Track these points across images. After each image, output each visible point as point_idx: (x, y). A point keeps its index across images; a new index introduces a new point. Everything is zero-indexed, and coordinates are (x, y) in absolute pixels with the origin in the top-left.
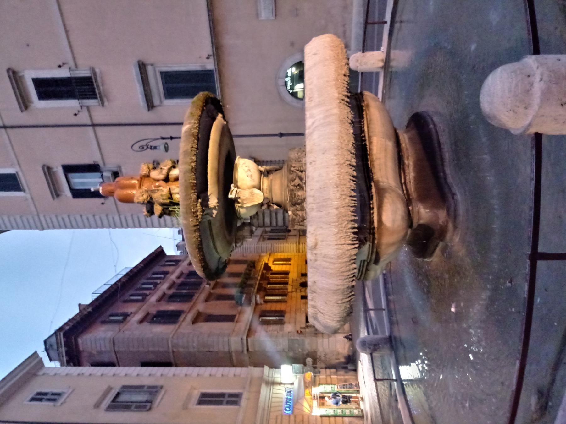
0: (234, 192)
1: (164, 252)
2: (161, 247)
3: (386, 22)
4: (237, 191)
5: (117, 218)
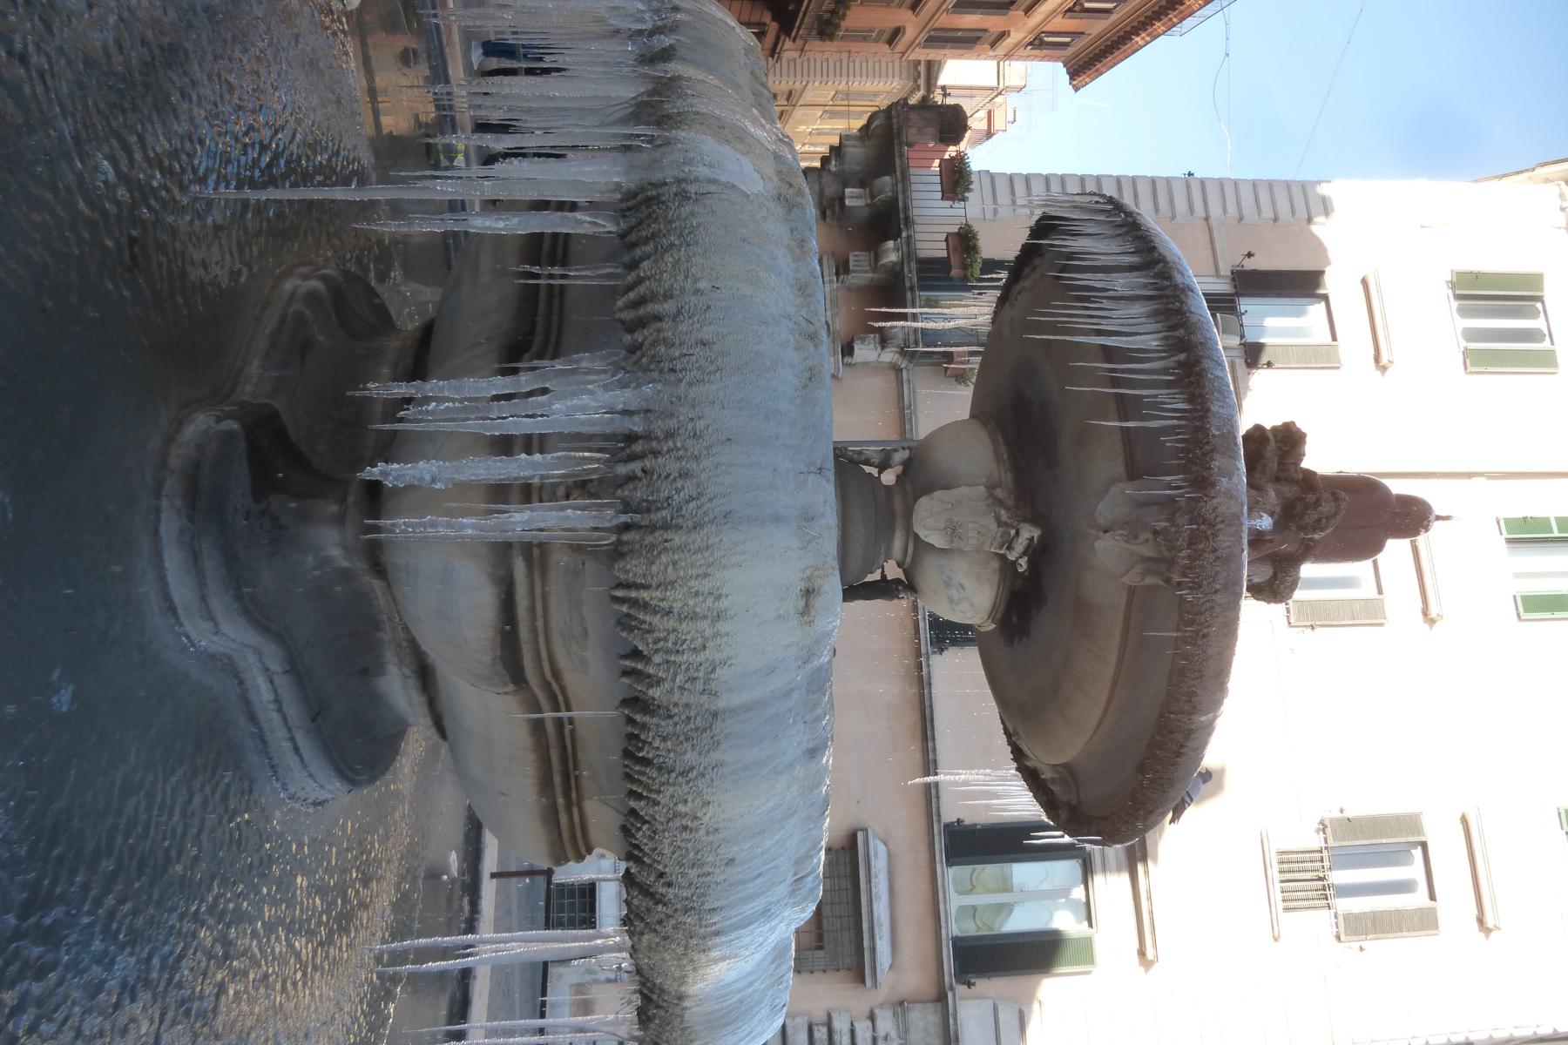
0: (1020, 545)
1: (1068, 73)
2: (1076, 89)
3: (493, 876)
4: (1010, 548)
5: (1215, 209)
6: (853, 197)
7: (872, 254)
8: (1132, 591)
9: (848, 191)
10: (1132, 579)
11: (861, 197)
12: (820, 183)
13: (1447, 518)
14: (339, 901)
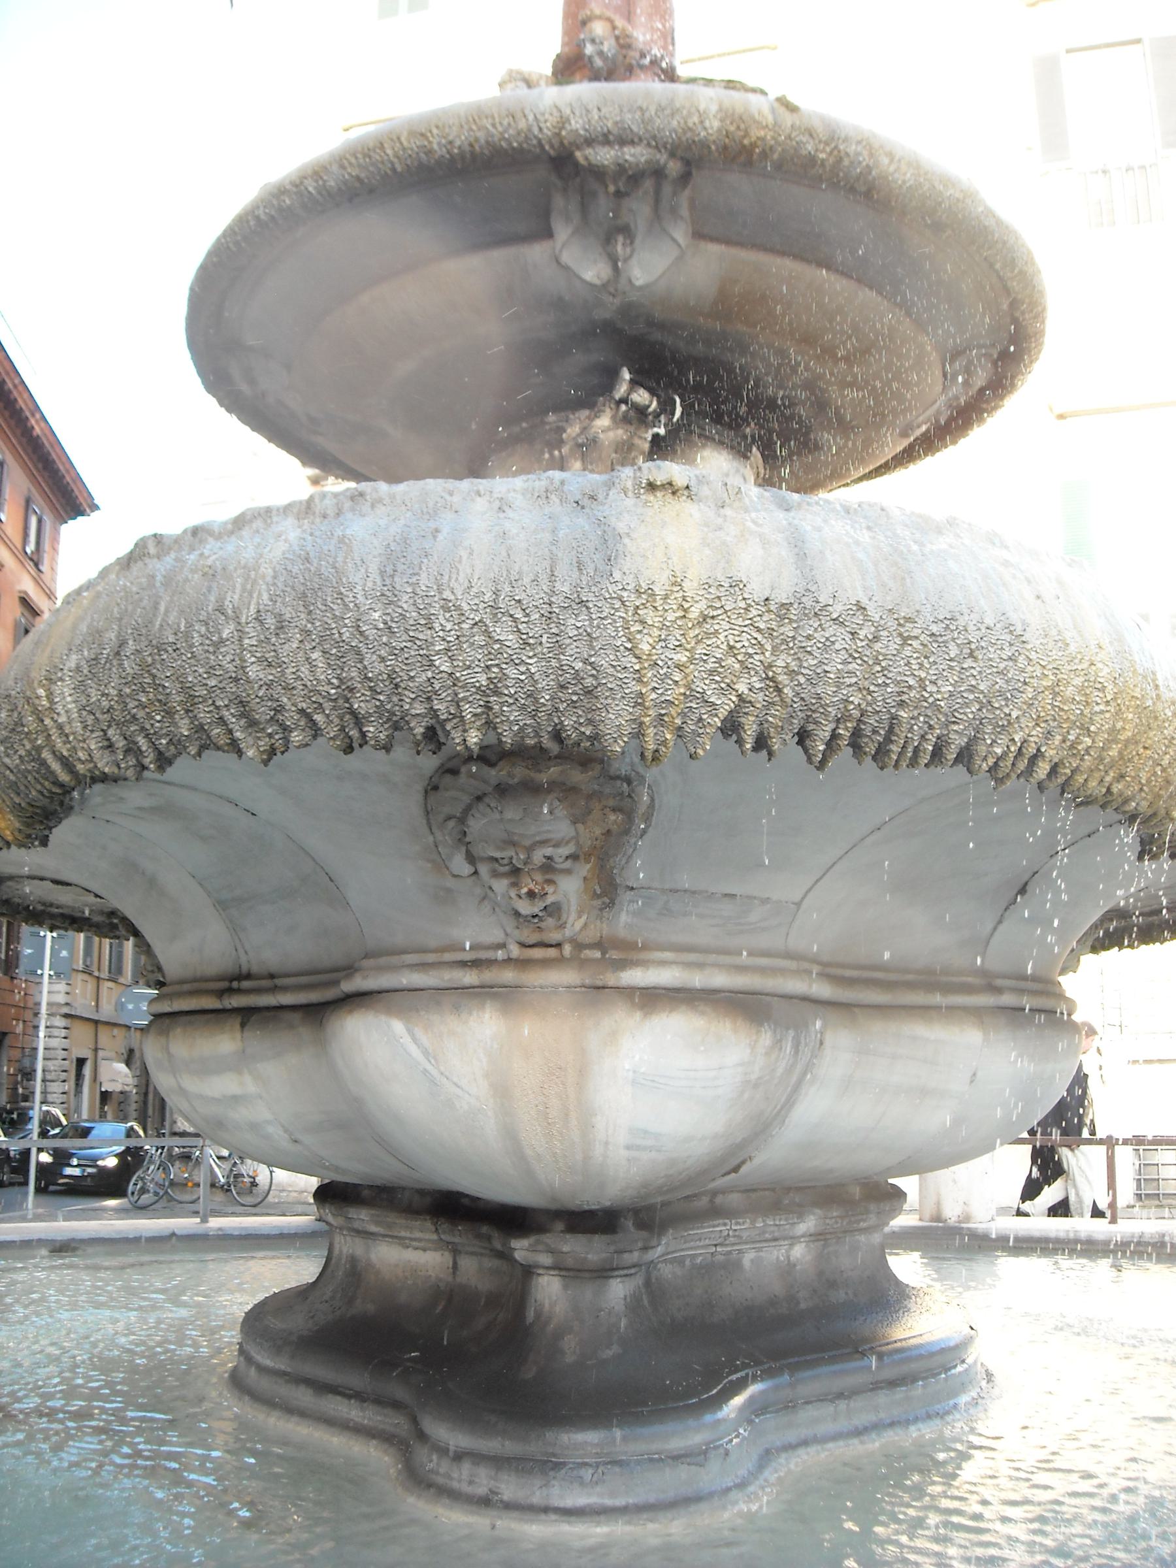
2: (95, 507)
8: (699, 235)
10: (680, 233)
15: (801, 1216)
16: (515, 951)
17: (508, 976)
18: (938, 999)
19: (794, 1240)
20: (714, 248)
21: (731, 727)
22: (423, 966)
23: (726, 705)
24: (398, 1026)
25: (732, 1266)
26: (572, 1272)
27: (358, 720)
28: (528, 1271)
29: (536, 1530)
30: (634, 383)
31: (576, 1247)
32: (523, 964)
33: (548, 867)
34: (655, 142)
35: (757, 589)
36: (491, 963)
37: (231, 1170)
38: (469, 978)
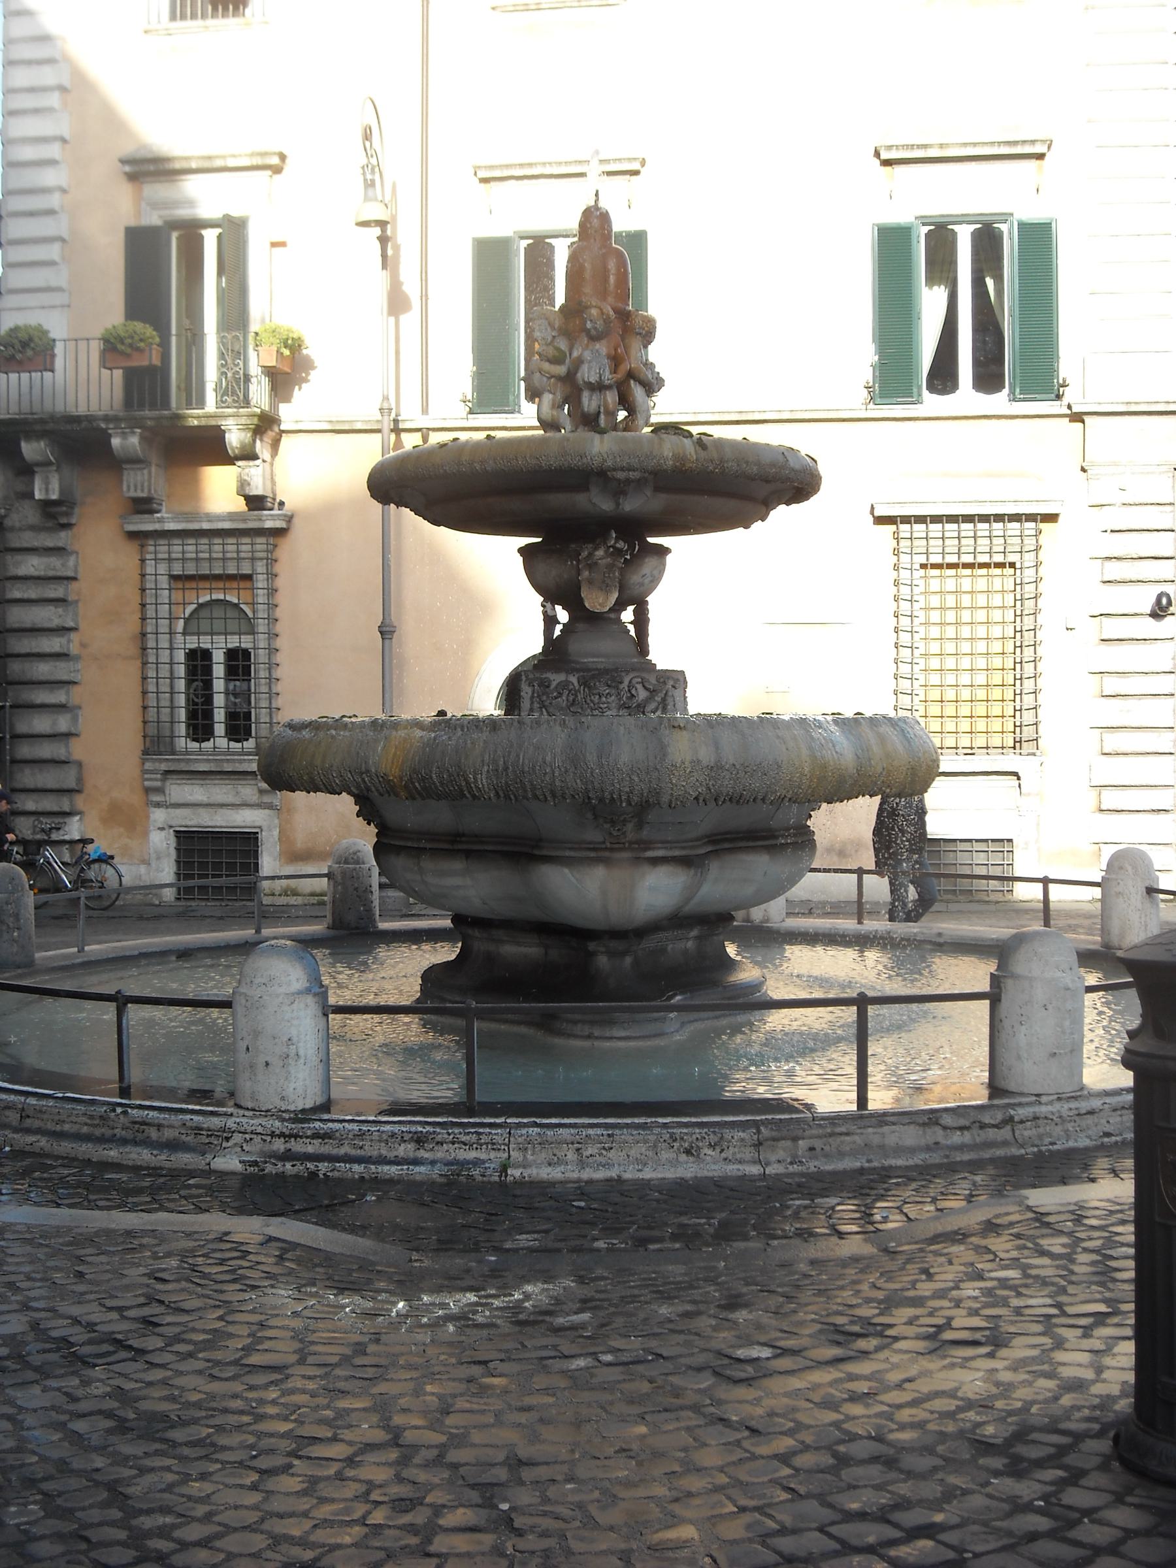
6: (47, 490)
7: (128, 466)
9: (37, 496)
11: (47, 477)
12: (20, 529)
13: (597, 195)
14: (582, 1204)
15: (692, 930)
16: (608, 845)
17: (607, 854)
18: (751, 844)
19: (688, 939)
20: (663, 496)
21: (696, 798)
22: (571, 849)
23: (695, 794)
24: (566, 871)
25: (663, 951)
26: (612, 954)
27: (589, 798)
28: (593, 954)
29: (608, 1044)
30: (617, 539)
31: (614, 944)
32: (612, 850)
33: (624, 820)
34: (645, 471)
35: (705, 762)
36: (601, 849)
37: (79, 876)
38: (592, 854)
